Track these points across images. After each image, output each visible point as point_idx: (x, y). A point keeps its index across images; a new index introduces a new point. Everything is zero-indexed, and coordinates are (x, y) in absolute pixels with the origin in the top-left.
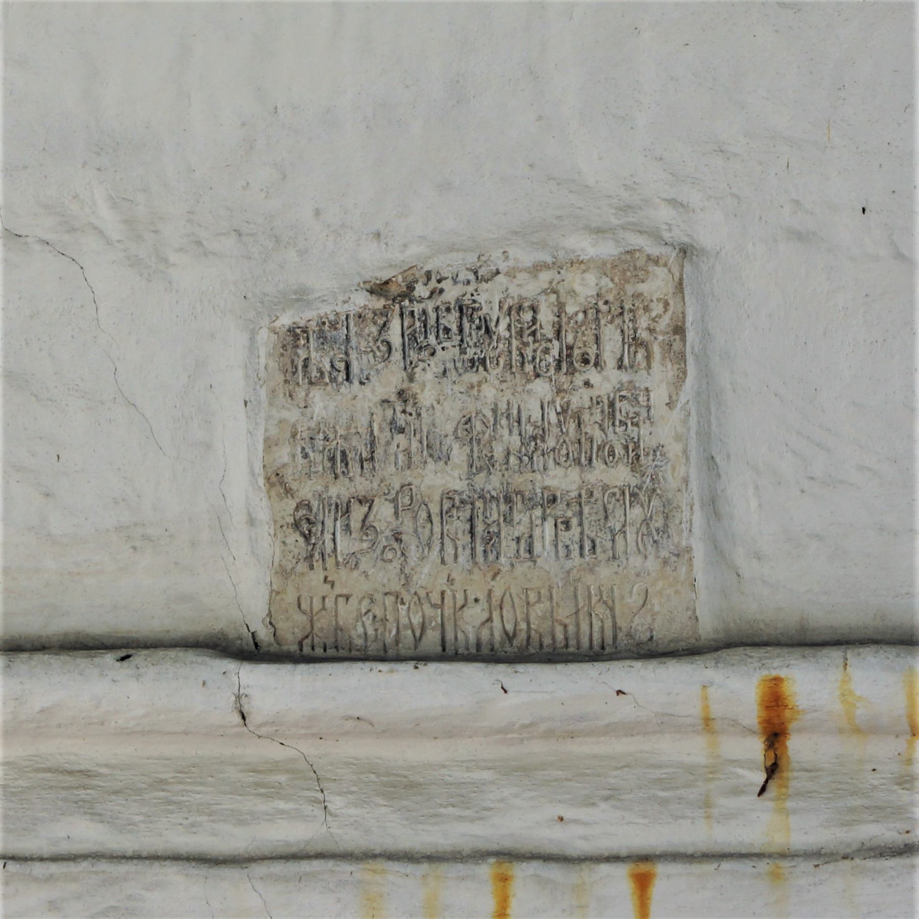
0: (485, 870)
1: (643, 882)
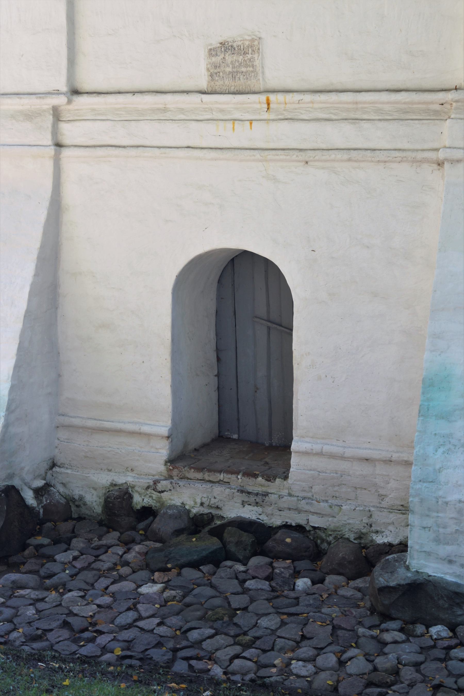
0: (232, 122)
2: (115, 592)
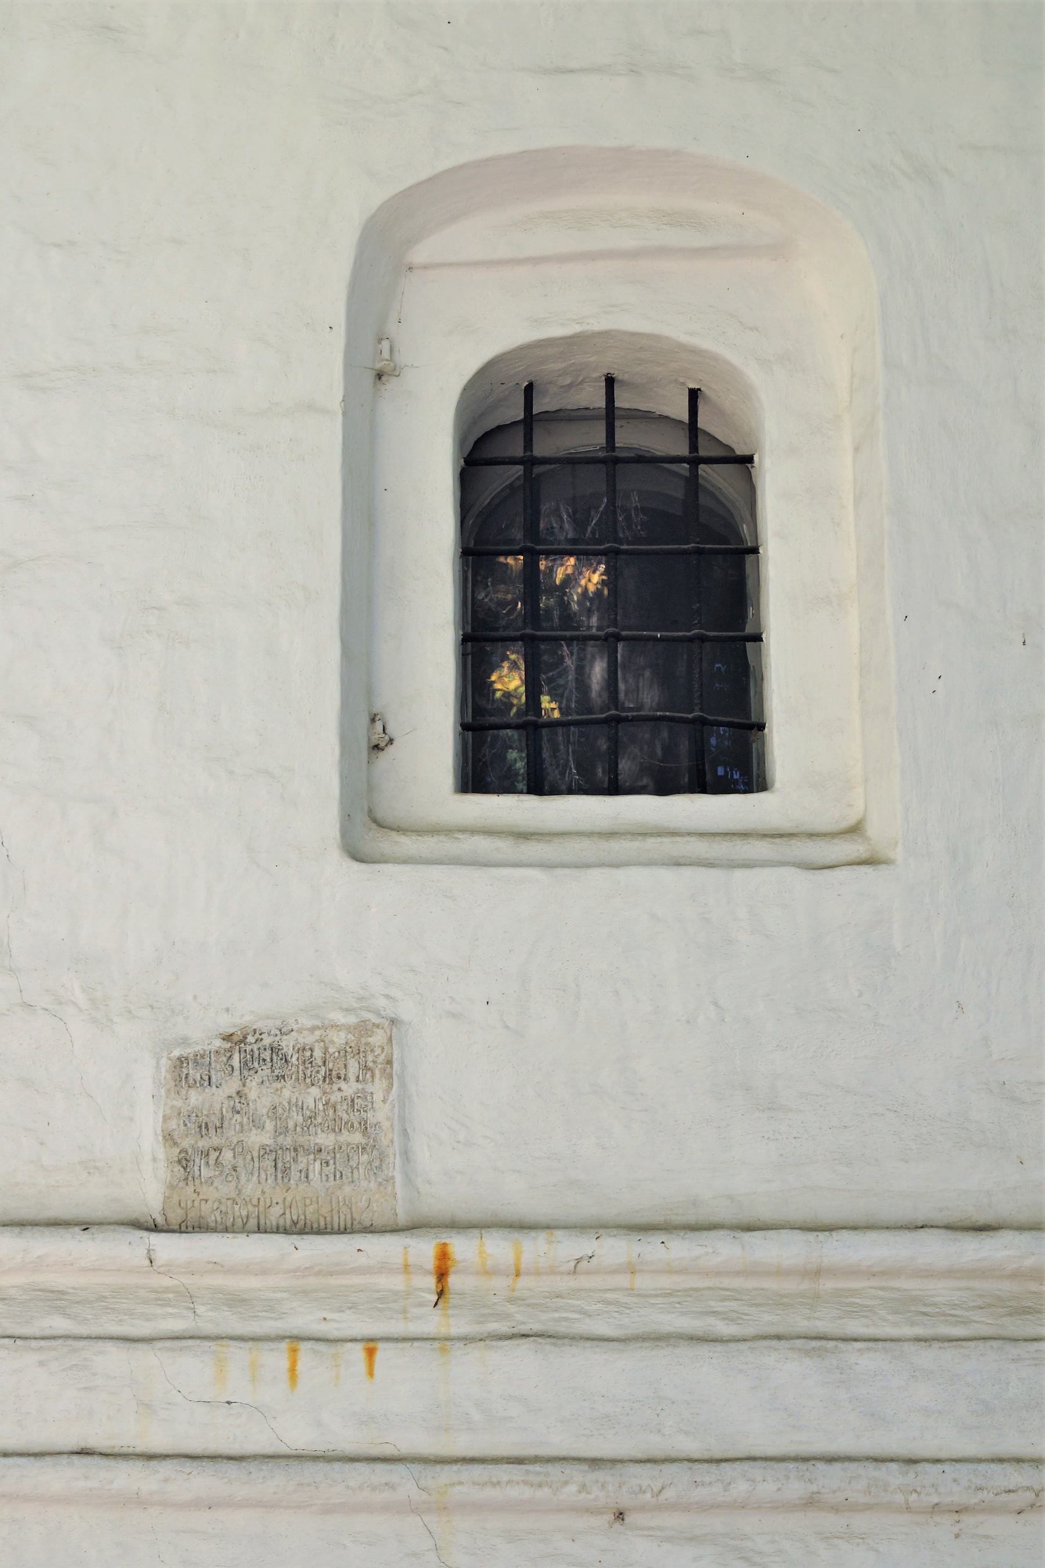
1: (371, 1353)
2: (462, 792)
